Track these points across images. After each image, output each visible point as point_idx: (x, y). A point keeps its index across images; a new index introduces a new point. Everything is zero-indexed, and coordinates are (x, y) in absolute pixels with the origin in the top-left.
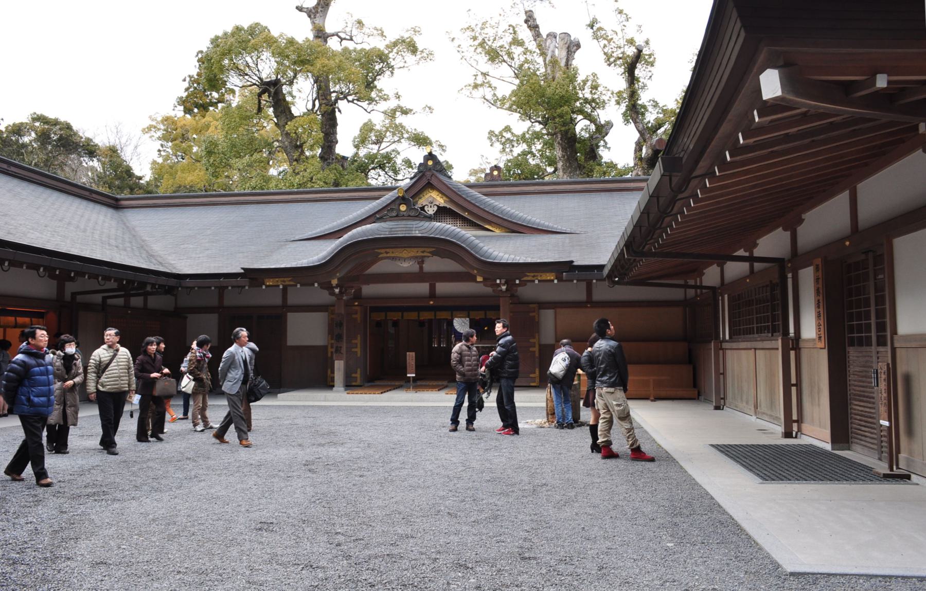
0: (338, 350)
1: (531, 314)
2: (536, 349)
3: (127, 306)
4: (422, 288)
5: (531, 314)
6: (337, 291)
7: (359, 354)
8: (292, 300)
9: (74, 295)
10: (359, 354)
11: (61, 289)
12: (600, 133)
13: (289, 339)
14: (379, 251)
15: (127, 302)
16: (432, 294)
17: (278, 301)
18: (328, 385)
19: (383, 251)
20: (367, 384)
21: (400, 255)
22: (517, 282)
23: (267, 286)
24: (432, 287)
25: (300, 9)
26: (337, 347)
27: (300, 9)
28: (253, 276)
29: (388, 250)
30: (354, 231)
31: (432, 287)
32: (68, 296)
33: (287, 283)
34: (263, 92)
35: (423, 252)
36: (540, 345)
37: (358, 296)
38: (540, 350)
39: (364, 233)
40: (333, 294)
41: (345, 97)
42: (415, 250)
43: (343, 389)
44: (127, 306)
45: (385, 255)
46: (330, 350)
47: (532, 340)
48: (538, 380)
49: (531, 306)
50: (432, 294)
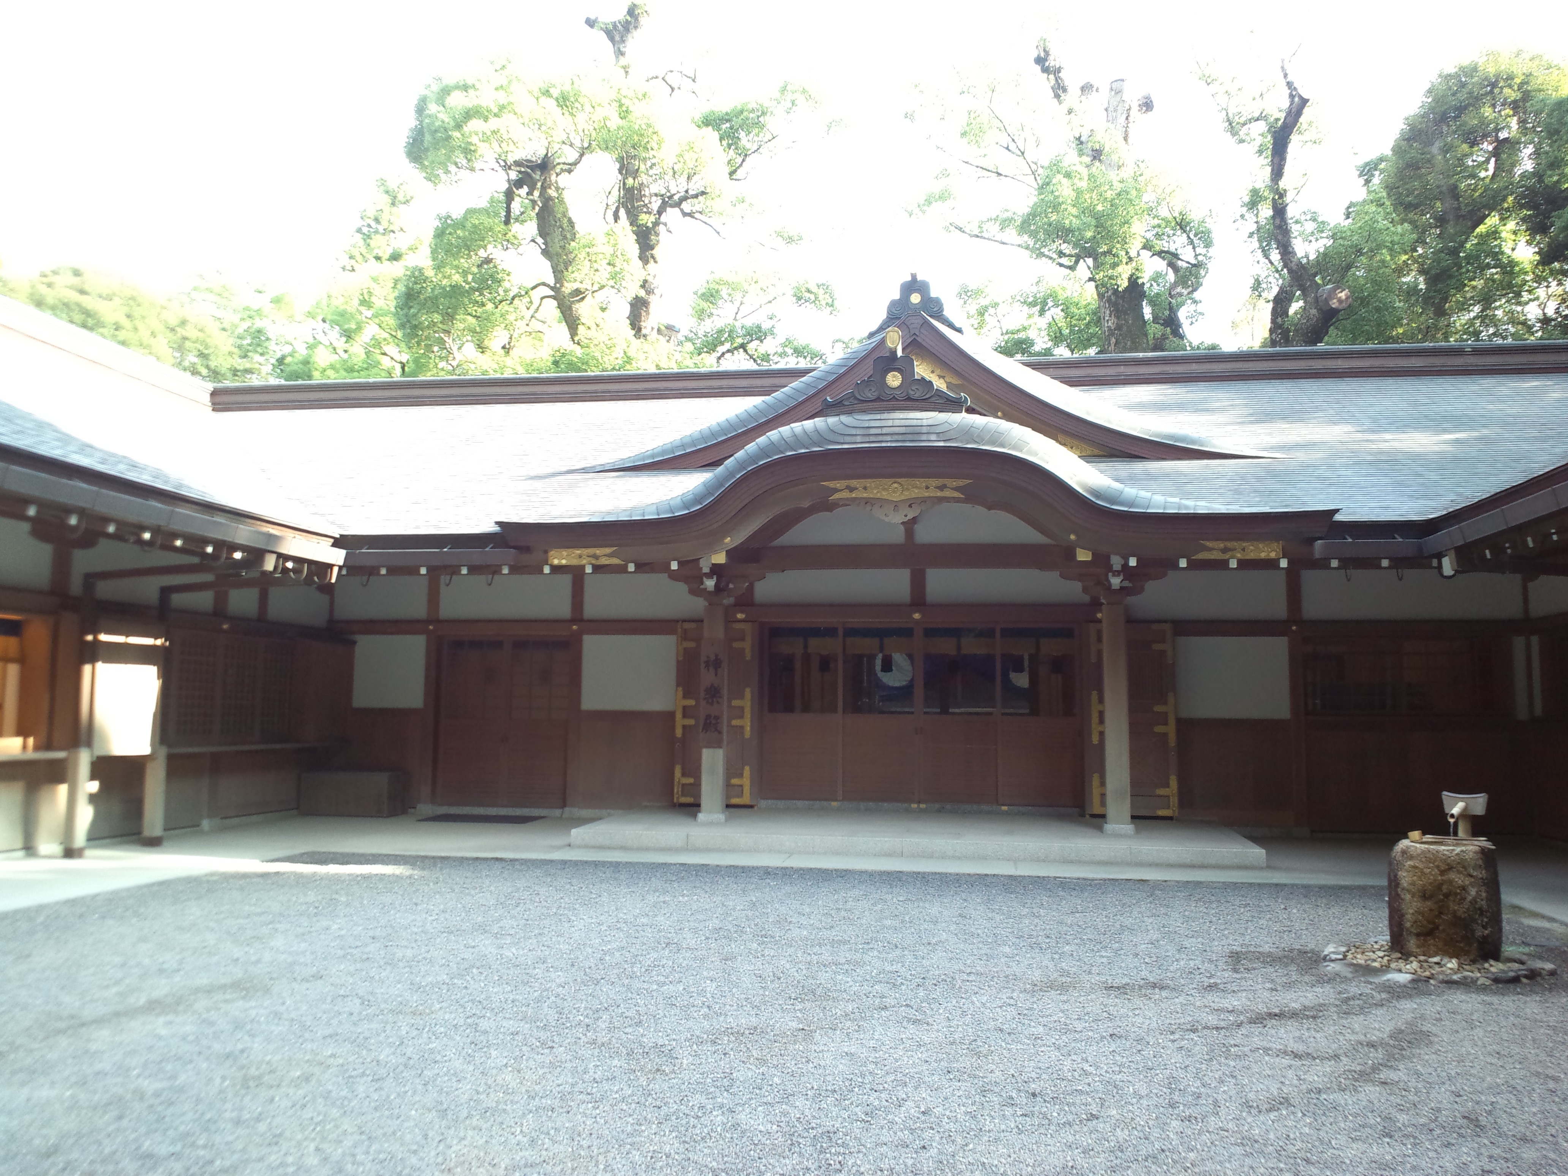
0: (711, 725)
1: (1157, 647)
2: (1170, 729)
3: (219, 612)
4: (891, 584)
5: (1157, 647)
6: (710, 584)
7: (747, 735)
8: (592, 608)
9: (90, 579)
10: (747, 735)
11: (62, 564)
12: (1185, 285)
13: (1276, 716)
14: (831, 484)
15: (221, 599)
16: (918, 600)
17: (562, 608)
18: (690, 808)
19: (838, 484)
20: (763, 803)
21: (885, 495)
22: (1183, 563)
23: (556, 569)
24: (918, 582)
25: (591, 23)
26: (708, 717)
27: (591, 23)
28: (519, 543)
29: (854, 483)
30: (773, 435)
31: (918, 582)
32: (76, 586)
33: (604, 561)
34: (519, 184)
35: (942, 488)
36: (1180, 722)
37: (746, 602)
38: (1179, 731)
39: (819, 436)
40: (697, 590)
41: (678, 204)
42: (921, 482)
43: (721, 817)
44: (219, 612)
45: (845, 494)
46: (680, 721)
47: (1158, 708)
48: (1174, 801)
49: (1155, 627)
50: (918, 600)
